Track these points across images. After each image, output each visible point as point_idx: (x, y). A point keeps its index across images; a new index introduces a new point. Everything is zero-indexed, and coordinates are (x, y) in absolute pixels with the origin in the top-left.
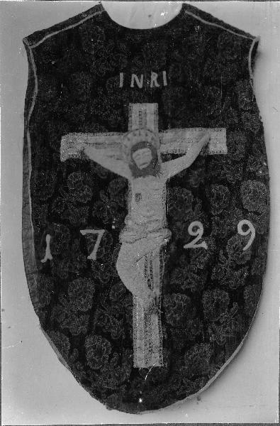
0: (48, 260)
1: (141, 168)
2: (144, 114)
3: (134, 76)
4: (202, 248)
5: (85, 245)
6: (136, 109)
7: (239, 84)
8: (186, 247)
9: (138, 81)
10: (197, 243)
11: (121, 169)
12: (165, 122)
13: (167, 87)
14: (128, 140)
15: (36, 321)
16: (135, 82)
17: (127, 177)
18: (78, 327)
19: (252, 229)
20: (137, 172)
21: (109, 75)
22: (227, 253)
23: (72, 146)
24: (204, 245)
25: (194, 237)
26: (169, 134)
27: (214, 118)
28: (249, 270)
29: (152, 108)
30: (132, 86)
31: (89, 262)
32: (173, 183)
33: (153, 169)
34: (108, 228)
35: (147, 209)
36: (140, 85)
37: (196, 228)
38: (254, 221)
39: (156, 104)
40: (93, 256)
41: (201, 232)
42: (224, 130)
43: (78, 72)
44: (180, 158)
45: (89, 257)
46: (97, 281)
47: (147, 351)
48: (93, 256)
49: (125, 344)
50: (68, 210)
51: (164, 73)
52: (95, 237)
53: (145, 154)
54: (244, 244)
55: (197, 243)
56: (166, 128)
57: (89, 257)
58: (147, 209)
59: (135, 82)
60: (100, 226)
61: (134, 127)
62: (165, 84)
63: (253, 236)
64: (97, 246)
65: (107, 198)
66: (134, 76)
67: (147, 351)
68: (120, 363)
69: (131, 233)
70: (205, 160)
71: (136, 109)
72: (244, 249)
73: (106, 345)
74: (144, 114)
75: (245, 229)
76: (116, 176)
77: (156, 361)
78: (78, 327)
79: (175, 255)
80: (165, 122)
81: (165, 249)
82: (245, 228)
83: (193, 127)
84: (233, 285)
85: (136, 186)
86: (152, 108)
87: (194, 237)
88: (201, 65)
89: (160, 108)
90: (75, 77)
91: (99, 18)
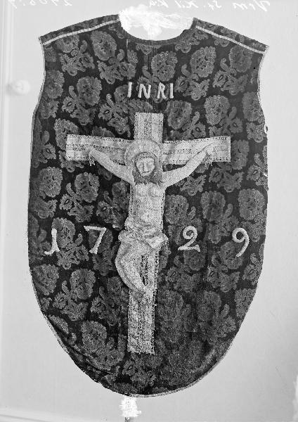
0: (55, 252)
2: (148, 124)
3: (142, 86)
4: (196, 251)
7: (247, 97)
8: (181, 248)
10: (191, 246)
11: (126, 174)
12: (170, 134)
15: (268, 141)
19: (247, 237)
20: (137, 182)
21: (118, 84)
22: (183, 258)
24: (197, 248)
25: (187, 241)
28: (241, 275)
29: (158, 118)
30: (140, 96)
31: (91, 255)
32: (171, 191)
33: (153, 179)
34: (109, 226)
35: (149, 206)
36: (148, 96)
38: (247, 230)
40: (95, 250)
42: (229, 138)
43: (92, 77)
44: (179, 169)
45: (91, 251)
46: (103, 82)
47: (141, 339)
48: (95, 250)
50: (73, 211)
51: (172, 85)
52: (98, 233)
54: (236, 251)
55: (191, 246)
57: (91, 251)
58: (149, 206)
59: (143, 93)
60: (102, 224)
61: (139, 136)
62: (172, 97)
63: (247, 244)
66: (142, 86)
67: (141, 339)
71: (140, 118)
73: (102, 330)
74: (148, 124)
79: (172, 256)
80: (170, 134)
82: (240, 235)
84: (224, 288)
85: (141, 189)
87: (187, 241)
90: (92, 165)
91: (111, 27)
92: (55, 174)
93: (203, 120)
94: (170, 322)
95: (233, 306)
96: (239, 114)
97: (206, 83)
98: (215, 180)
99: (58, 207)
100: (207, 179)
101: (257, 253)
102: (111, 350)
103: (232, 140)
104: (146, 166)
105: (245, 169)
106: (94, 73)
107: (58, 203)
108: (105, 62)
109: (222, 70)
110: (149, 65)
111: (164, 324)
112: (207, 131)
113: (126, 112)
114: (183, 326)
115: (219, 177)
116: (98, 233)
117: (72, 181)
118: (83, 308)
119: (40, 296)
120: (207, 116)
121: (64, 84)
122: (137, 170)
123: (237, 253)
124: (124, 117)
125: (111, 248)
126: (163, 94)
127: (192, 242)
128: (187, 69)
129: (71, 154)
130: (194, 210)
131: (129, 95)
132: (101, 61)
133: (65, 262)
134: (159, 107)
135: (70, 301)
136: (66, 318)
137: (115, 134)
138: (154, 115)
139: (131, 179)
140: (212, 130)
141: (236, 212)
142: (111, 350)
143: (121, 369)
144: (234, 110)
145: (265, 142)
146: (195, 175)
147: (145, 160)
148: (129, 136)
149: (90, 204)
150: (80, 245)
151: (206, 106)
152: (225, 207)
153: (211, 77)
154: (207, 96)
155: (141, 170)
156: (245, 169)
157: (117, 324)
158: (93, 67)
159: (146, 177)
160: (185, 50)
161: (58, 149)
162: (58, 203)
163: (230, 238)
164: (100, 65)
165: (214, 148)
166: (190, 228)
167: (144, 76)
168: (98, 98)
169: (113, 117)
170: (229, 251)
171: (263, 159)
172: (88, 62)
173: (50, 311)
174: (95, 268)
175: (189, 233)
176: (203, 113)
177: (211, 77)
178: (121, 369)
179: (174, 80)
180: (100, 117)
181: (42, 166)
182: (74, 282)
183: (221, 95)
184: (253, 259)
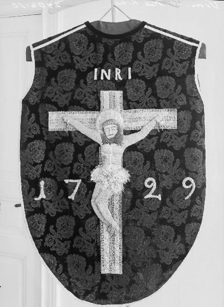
1: (108, 137)
2: (111, 98)
5: (67, 190)
6: (105, 95)
9: (106, 74)
11: (96, 137)
12: (128, 104)
13: (96, 257)
14: (100, 117)
16: (104, 75)
17: (99, 143)
18: (62, 249)
20: (105, 141)
23: (56, 121)
26: (131, 113)
27: (83, 57)
29: (119, 94)
32: (131, 149)
33: (116, 140)
35: (112, 155)
36: (108, 78)
37: (151, 183)
39: (122, 92)
41: (154, 185)
47: (111, 262)
48: (72, 197)
49: (95, 259)
50: (54, 166)
52: (76, 184)
53: (114, 124)
56: (129, 108)
58: (112, 155)
59: (104, 75)
60: (79, 179)
64: (76, 191)
65: (85, 153)
67: (111, 262)
68: (93, 272)
69: (121, 118)
70: (158, 135)
71: (105, 95)
72: (186, 199)
73: (82, 261)
74: (111, 98)
75: (189, 183)
76: (92, 142)
77: (118, 270)
78: (62, 249)
79: (133, 195)
81: (127, 186)
83: (149, 108)
86: (119, 94)
88: (153, 63)
89: (124, 94)
92: (40, 145)
93: (154, 94)
94: (136, 251)
95: (183, 236)
96: (184, 91)
97: (156, 66)
98: (166, 141)
99: (43, 170)
100: (159, 140)
101: (200, 196)
102: (90, 275)
103: (178, 112)
104: (111, 132)
105: (189, 133)
106: (70, 66)
107: (43, 167)
108: (78, 56)
109: (168, 57)
110: (113, 53)
111: (131, 252)
112: (158, 103)
113: (96, 91)
114: (145, 254)
115: (169, 138)
116: (76, 184)
117: (53, 149)
118: (62, 235)
119: (35, 239)
120: (158, 92)
121: (47, 77)
122: (105, 134)
123: (186, 196)
124: (93, 95)
125: (86, 197)
126: (119, 76)
127: (153, 190)
128: (141, 55)
129: (52, 127)
130: (148, 163)
131: (96, 78)
132: (76, 56)
133: (52, 210)
134: (119, 86)
135: (57, 240)
136: (54, 253)
137: (87, 108)
138: (117, 92)
139: (99, 140)
140: (162, 102)
141: (183, 166)
142: (90, 275)
143: (100, 288)
144: (180, 88)
145: (203, 113)
146: (150, 136)
147: (110, 126)
148: (96, 107)
149: (68, 166)
150: (62, 198)
151: (157, 84)
152: (170, 160)
153: (160, 62)
154: (157, 77)
155: (107, 134)
156: (189, 133)
157: (94, 255)
158: (70, 62)
159: (111, 139)
160: (139, 40)
161: (41, 126)
162: (43, 167)
163: (181, 184)
164: (75, 58)
165: (167, 118)
166: (149, 179)
167: (109, 62)
168: (74, 84)
169: (85, 96)
170: (180, 195)
171: (202, 125)
172: (66, 58)
173: (43, 250)
174: (46, 138)
175: (150, 183)
176: (154, 89)
177: (160, 62)
178: (100, 288)
179: (130, 65)
180: (75, 98)
181: (30, 140)
182: (59, 227)
183: (169, 76)
184: (198, 201)
